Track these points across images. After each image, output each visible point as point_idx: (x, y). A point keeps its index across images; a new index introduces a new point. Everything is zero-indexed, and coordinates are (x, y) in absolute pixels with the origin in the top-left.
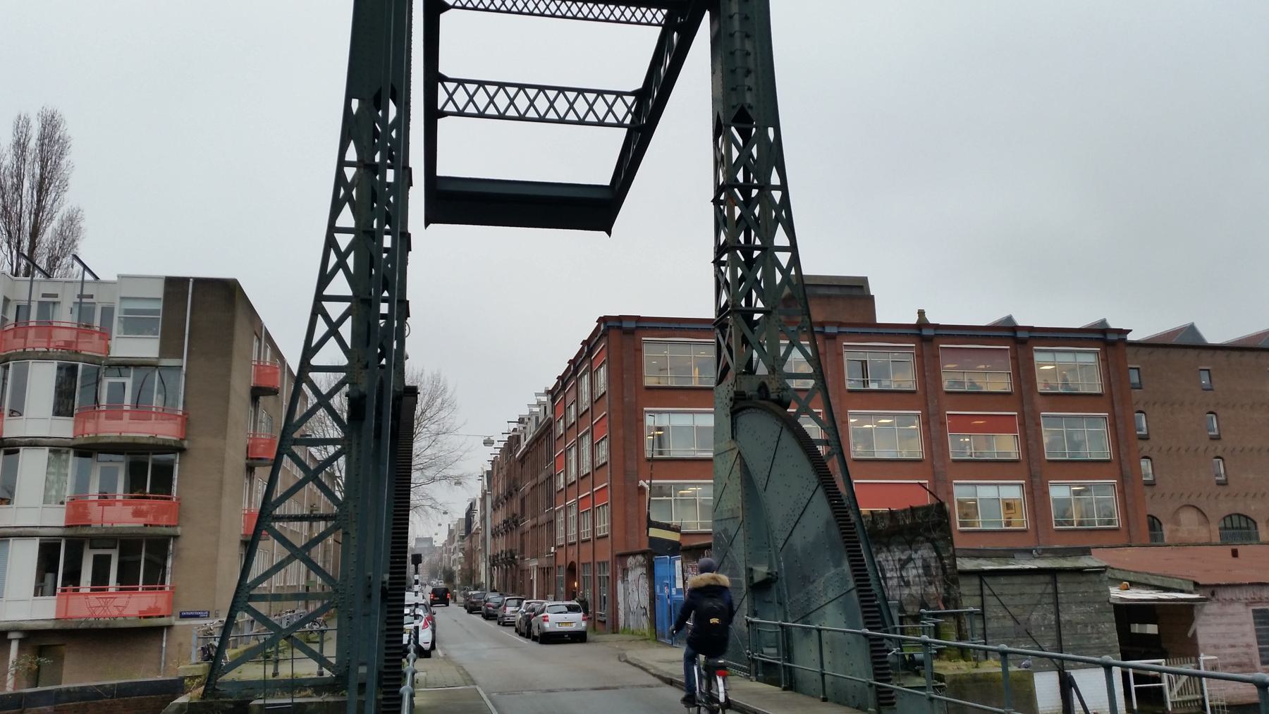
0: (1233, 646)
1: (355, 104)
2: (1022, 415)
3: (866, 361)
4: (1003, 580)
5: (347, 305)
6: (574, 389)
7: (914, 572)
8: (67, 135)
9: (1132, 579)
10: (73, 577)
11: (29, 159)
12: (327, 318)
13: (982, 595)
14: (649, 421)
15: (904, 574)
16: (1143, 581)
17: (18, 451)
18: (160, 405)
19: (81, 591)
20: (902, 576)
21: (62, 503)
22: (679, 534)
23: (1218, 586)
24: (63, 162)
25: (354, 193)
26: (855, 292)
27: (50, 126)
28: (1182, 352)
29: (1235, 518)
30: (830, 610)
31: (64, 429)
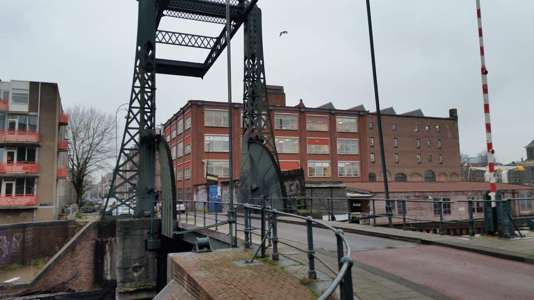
0: (379, 209)
1: (139, 48)
2: (331, 139)
3: (282, 119)
4: (317, 190)
5: (139, 110)
6: (175, 125)
7: (294, 187)
9: (355, 191)
13: (312, 194)
14: (207, 138)
15: (291, 188)
16: (357, 191)
20: (290, 189)
22: (217, 178)
23: (377, 192)
25: (140, 76)
26: (279, 92)
28: (388, 117)
29: (372, 174)
30: (274, 194)
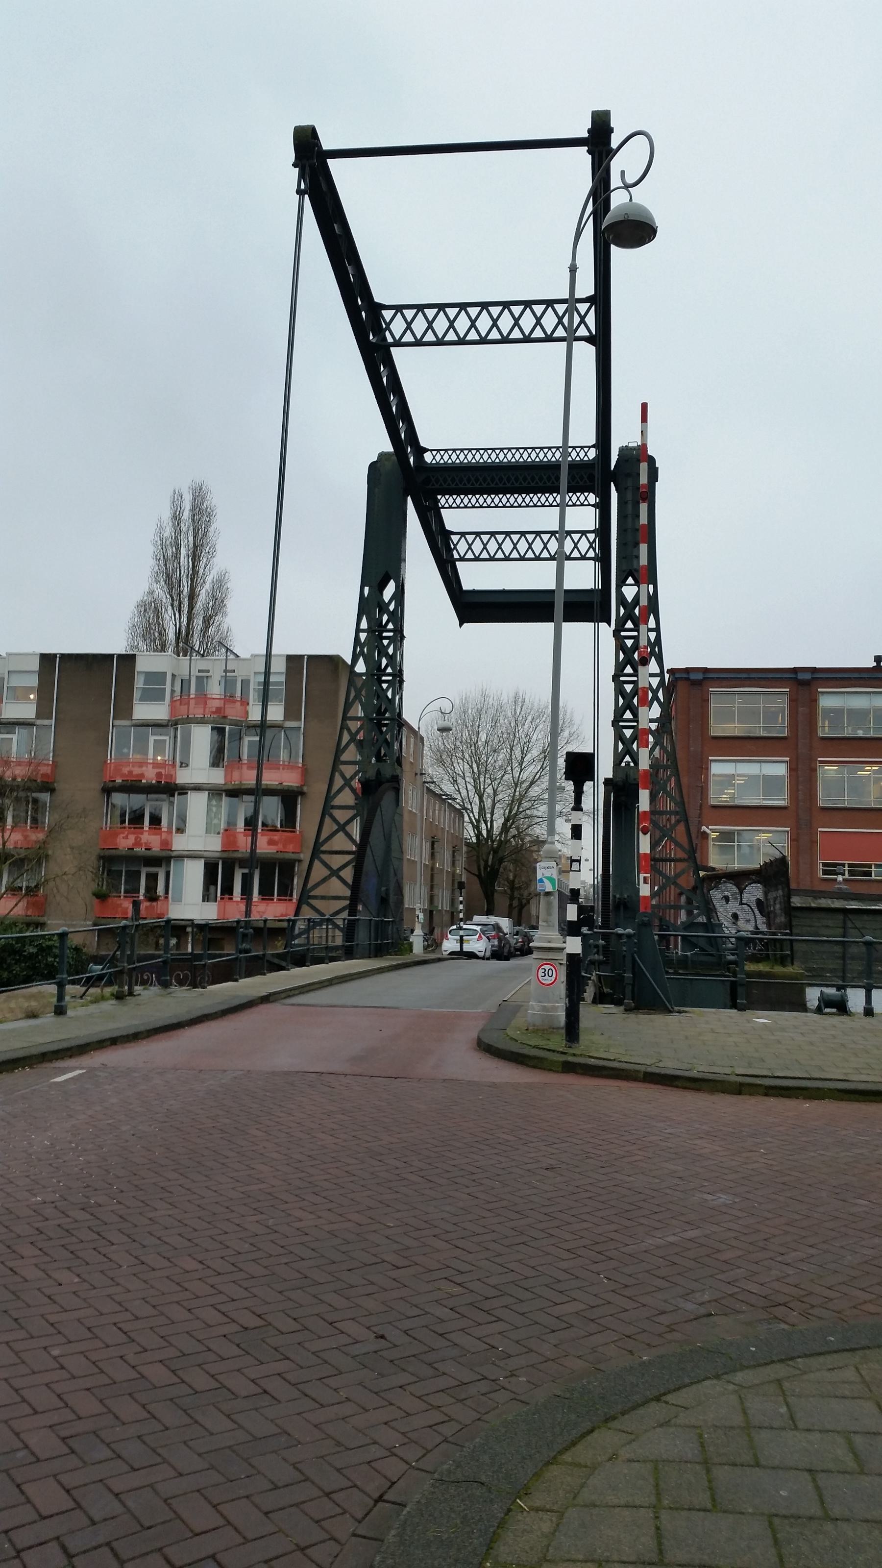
1: (366, 590)
4: (866, 917)
8: (213, 504)
10: (228, 890)
11: (184, 528)
12: (349, 730)
13: (844, 928)
17: (187, 793)
18: (287, 759)
19: (234, 899)
21: (219, 833)
24: (211, 529)
27: (199, 495)
31: (217, 777)
